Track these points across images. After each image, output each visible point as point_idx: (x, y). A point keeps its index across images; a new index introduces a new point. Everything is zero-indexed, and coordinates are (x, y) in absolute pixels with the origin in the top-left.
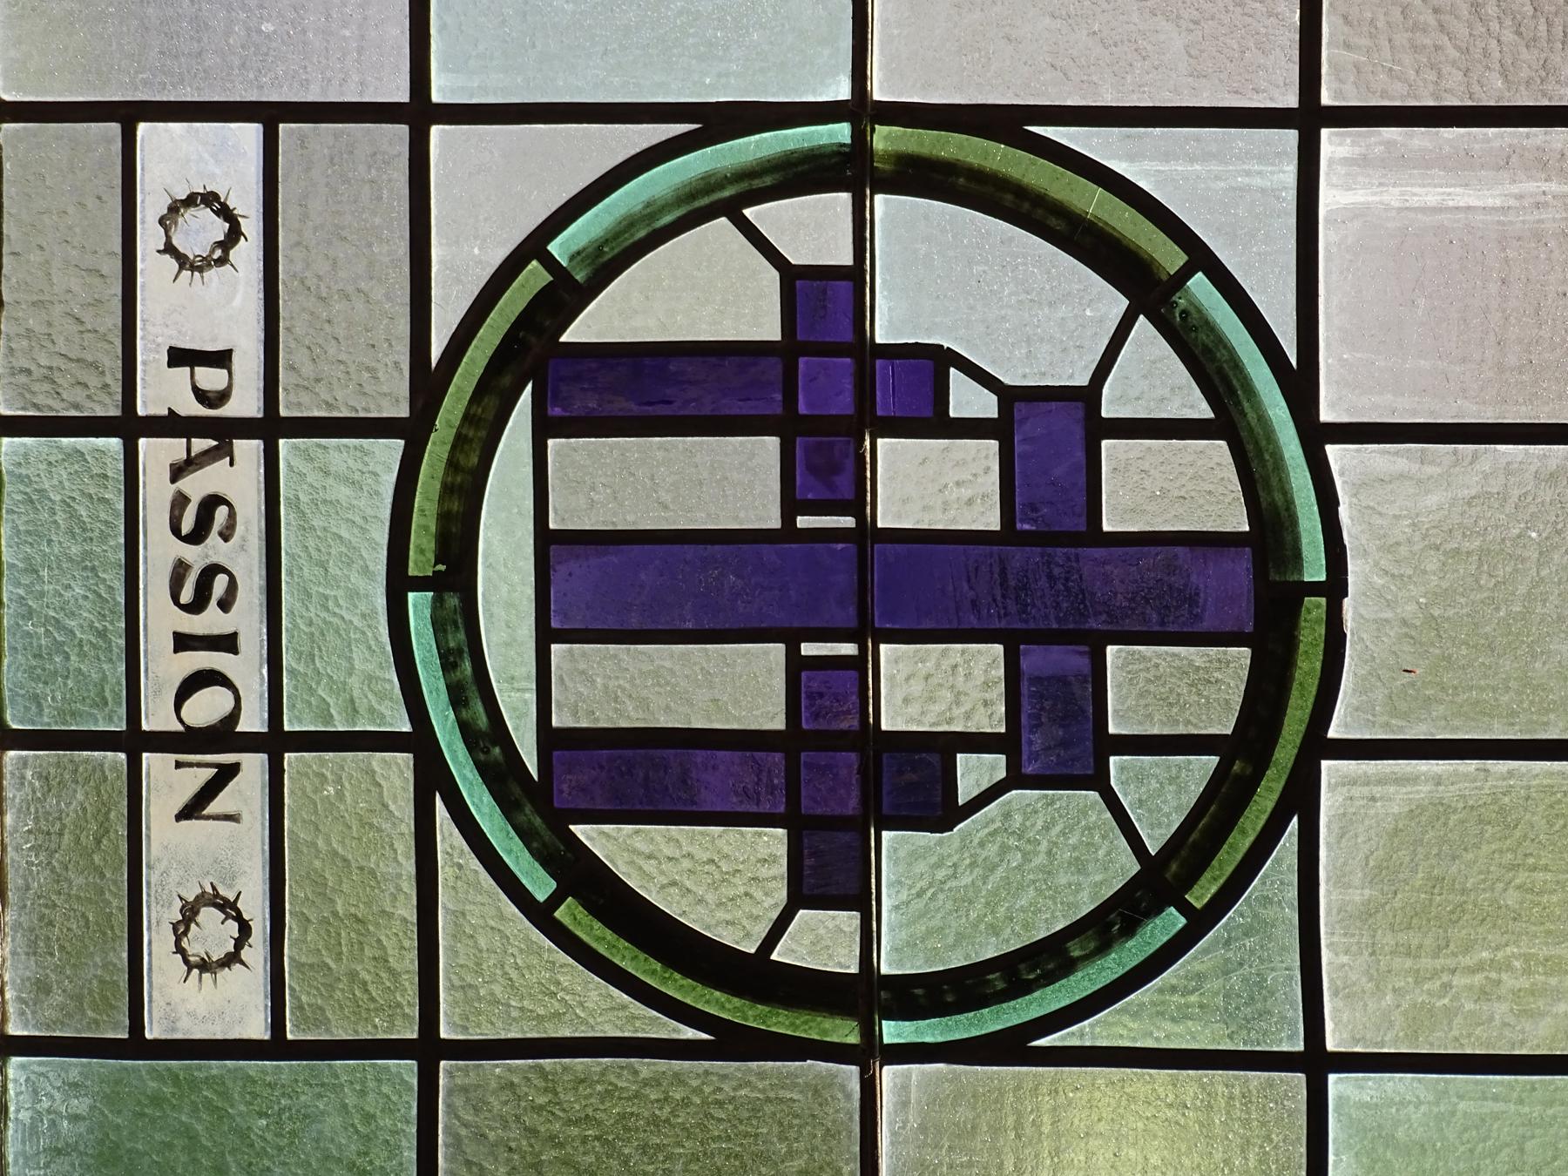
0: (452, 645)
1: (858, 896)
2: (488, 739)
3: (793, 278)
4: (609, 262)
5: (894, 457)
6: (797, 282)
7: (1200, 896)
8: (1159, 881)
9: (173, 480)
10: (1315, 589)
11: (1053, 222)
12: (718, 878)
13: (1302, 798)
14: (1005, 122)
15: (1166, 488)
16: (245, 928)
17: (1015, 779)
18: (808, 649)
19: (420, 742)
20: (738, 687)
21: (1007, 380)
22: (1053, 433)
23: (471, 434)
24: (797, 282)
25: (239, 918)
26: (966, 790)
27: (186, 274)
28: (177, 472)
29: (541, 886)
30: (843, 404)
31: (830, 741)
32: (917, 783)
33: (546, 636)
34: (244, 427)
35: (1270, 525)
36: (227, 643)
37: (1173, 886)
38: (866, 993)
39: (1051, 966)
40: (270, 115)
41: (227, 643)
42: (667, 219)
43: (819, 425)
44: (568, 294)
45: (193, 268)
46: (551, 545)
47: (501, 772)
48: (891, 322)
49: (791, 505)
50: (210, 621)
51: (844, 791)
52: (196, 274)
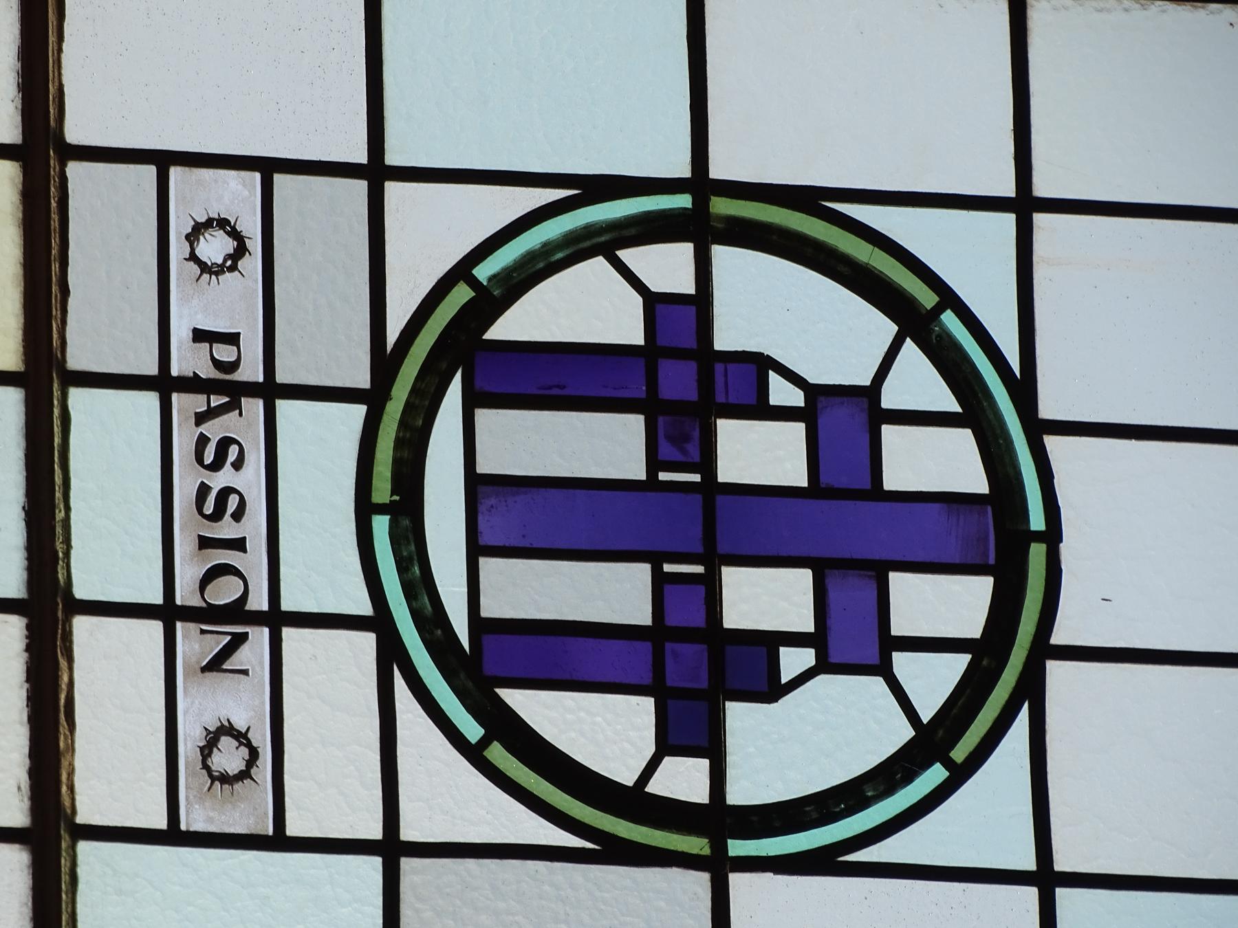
0: (405, 554)
1: (711, 746)
2: (432, 621)
3: (654, 302)
5: (728, 430)
6: (656, 304)
7: (959, 753)
9: (198, 424)
10: (1038, 536)
11: (842, 268)
12: (607, 731)
13: (1032, 689)
14: (807, 199)
15: (933, 461)
16: (254, 754)
17: (824, 666)
18: (668, 568)
20: (616, 593)
21: (812, 380)
22: (846, 418)
23: (417, 402)
24: (656, 304)
25: (249, 745)
26: (787, 674)
27: (206, 276)
28: (200, 419)
29: (473, 731)
30: (691, 393)
31: (686, 635)
32: (750, 666)
33: (476, 550)
34: (251, 389)
36: (239, 545)
37: (940, 748)
38: (719, 820)
39: (851, 803)
40: (268, 168)
41: (239, 545)
42: (559, 255)
43: (676, 408)
45: (211, 273)
46: (479, 486)
48: (728, 336)
49: (654, 464)
50: (226, 529)
52: (213, 277)
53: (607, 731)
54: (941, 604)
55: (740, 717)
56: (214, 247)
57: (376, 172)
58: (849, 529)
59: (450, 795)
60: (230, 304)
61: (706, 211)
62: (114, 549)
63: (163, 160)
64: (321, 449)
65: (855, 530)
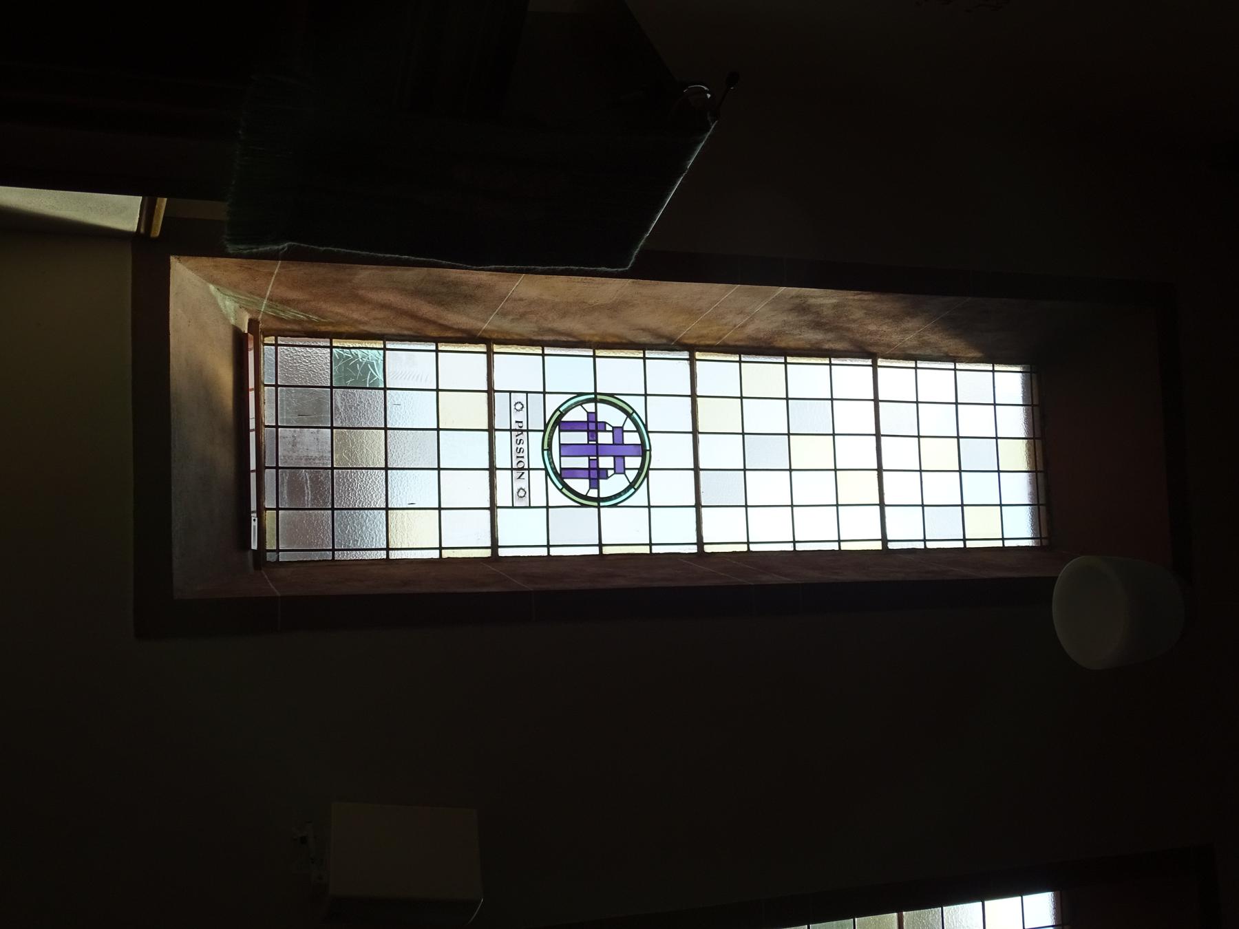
2: (554, 469)
4: (567, 411)
8: (632, 485)
12: (581, 485)
13: (647, 475)
15: (632, 438)
19: (546, 469)
20: (583, 462)
22: (618, 431)
35: (643, 444)
38: (599, 499)
44: (562, 415)
47: (554, 469)
51: (596, 475)
53: (581, 485)
54: (633, 462)
55: (601, 481)
56: (519, 407)
57: (544, 393)
58: (619, 450)
59: (557, 498)
60: (521, 416)
61: (596, 398)
62: (502, 460)
63: (510, 392)
64: (536, 439)
65: (619, 450)
